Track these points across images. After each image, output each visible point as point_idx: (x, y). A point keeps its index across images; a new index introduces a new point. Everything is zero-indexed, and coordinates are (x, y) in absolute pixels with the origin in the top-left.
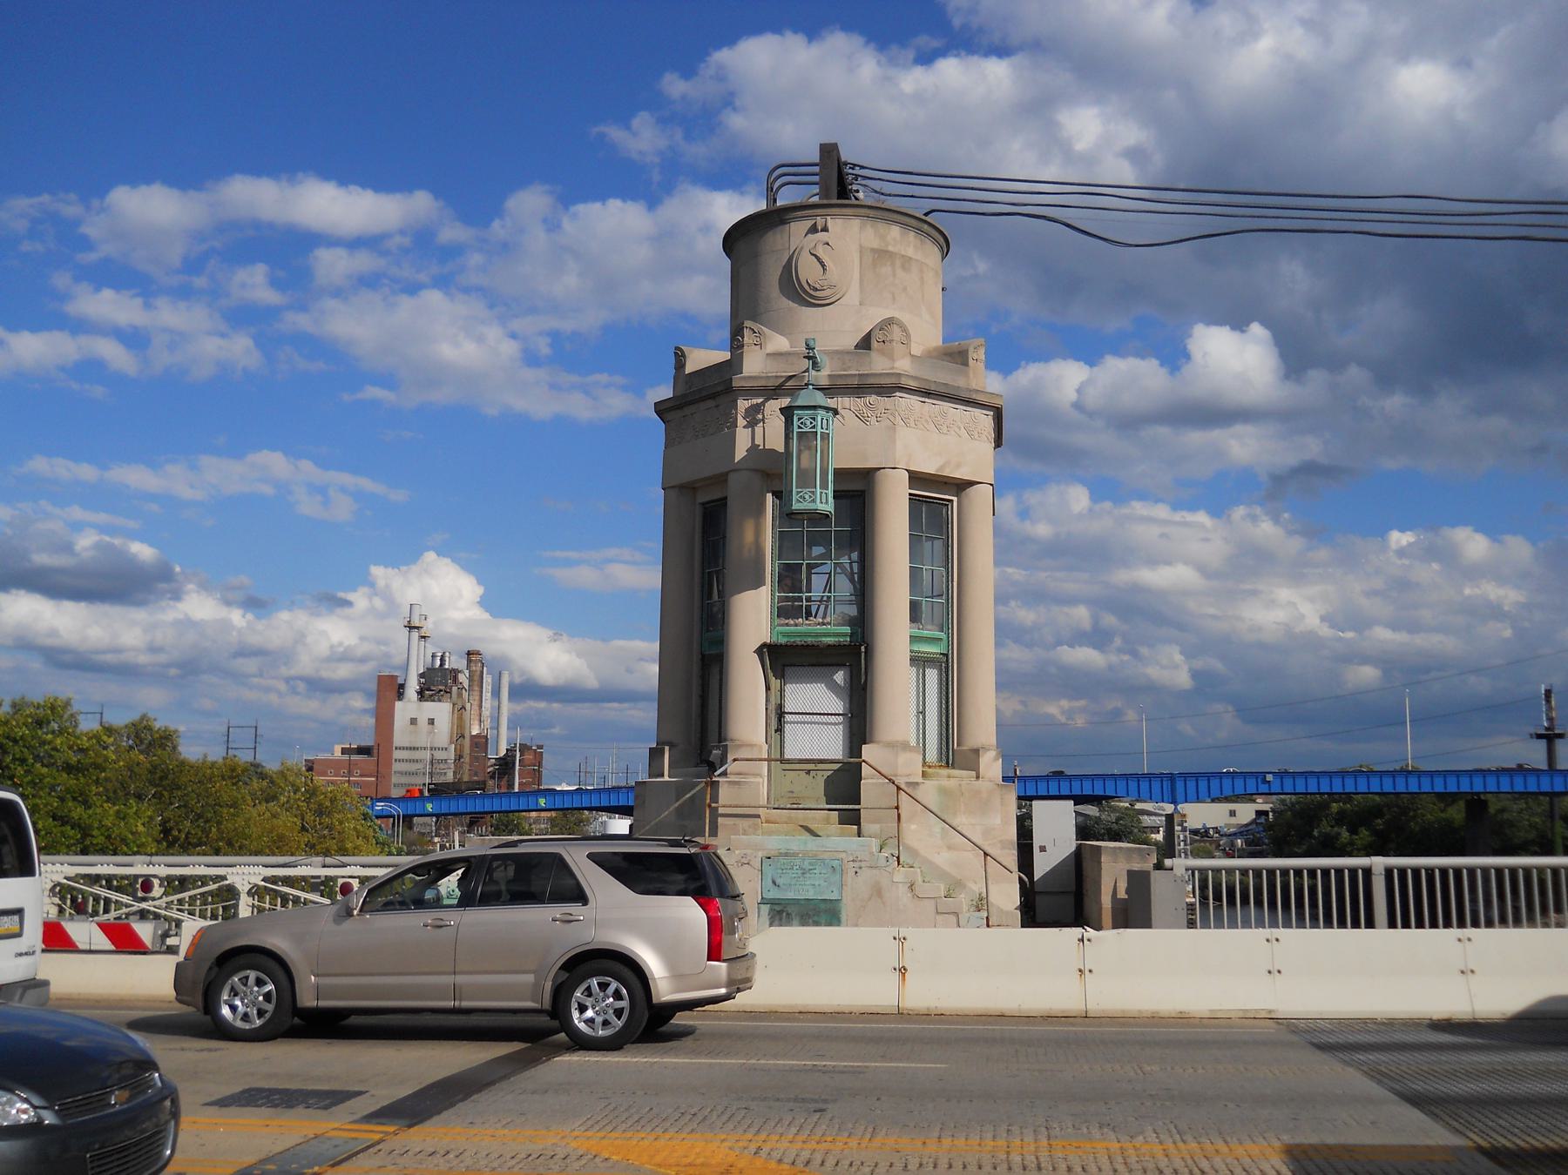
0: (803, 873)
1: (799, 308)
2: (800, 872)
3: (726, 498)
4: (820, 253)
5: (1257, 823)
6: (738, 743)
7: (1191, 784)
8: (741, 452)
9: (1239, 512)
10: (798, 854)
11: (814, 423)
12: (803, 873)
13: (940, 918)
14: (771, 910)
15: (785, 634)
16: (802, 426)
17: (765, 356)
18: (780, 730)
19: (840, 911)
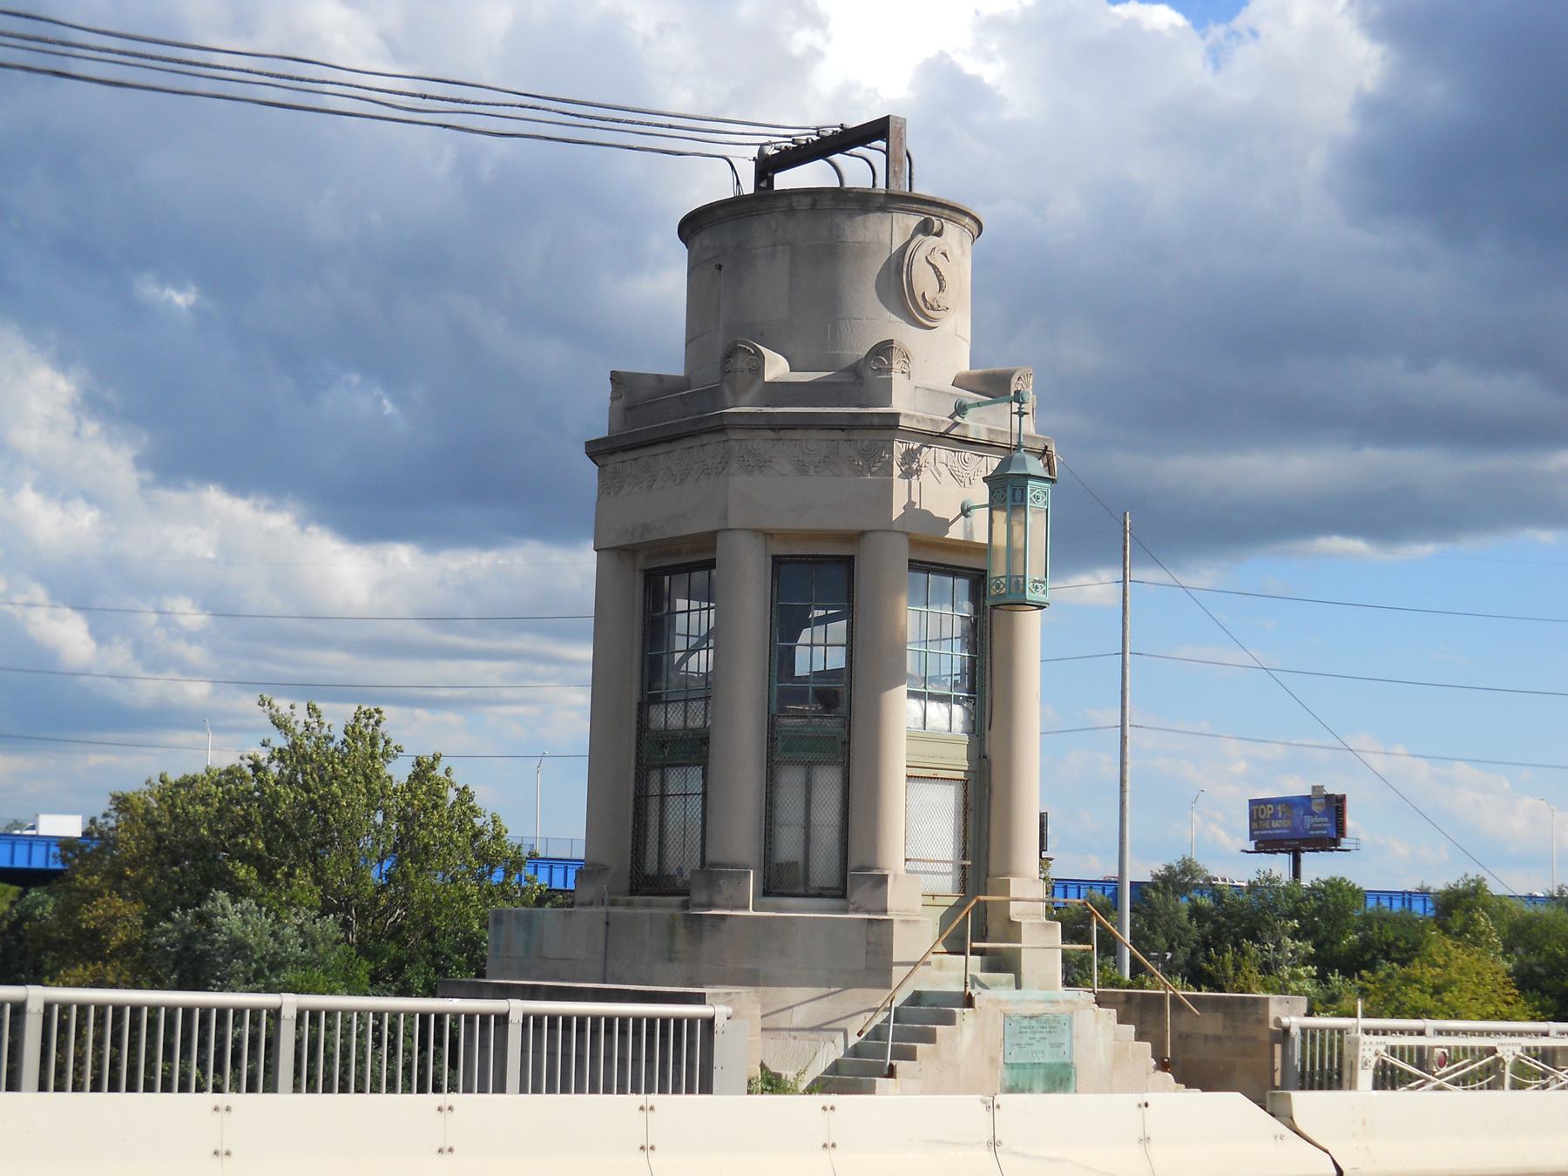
8: (897, 511)
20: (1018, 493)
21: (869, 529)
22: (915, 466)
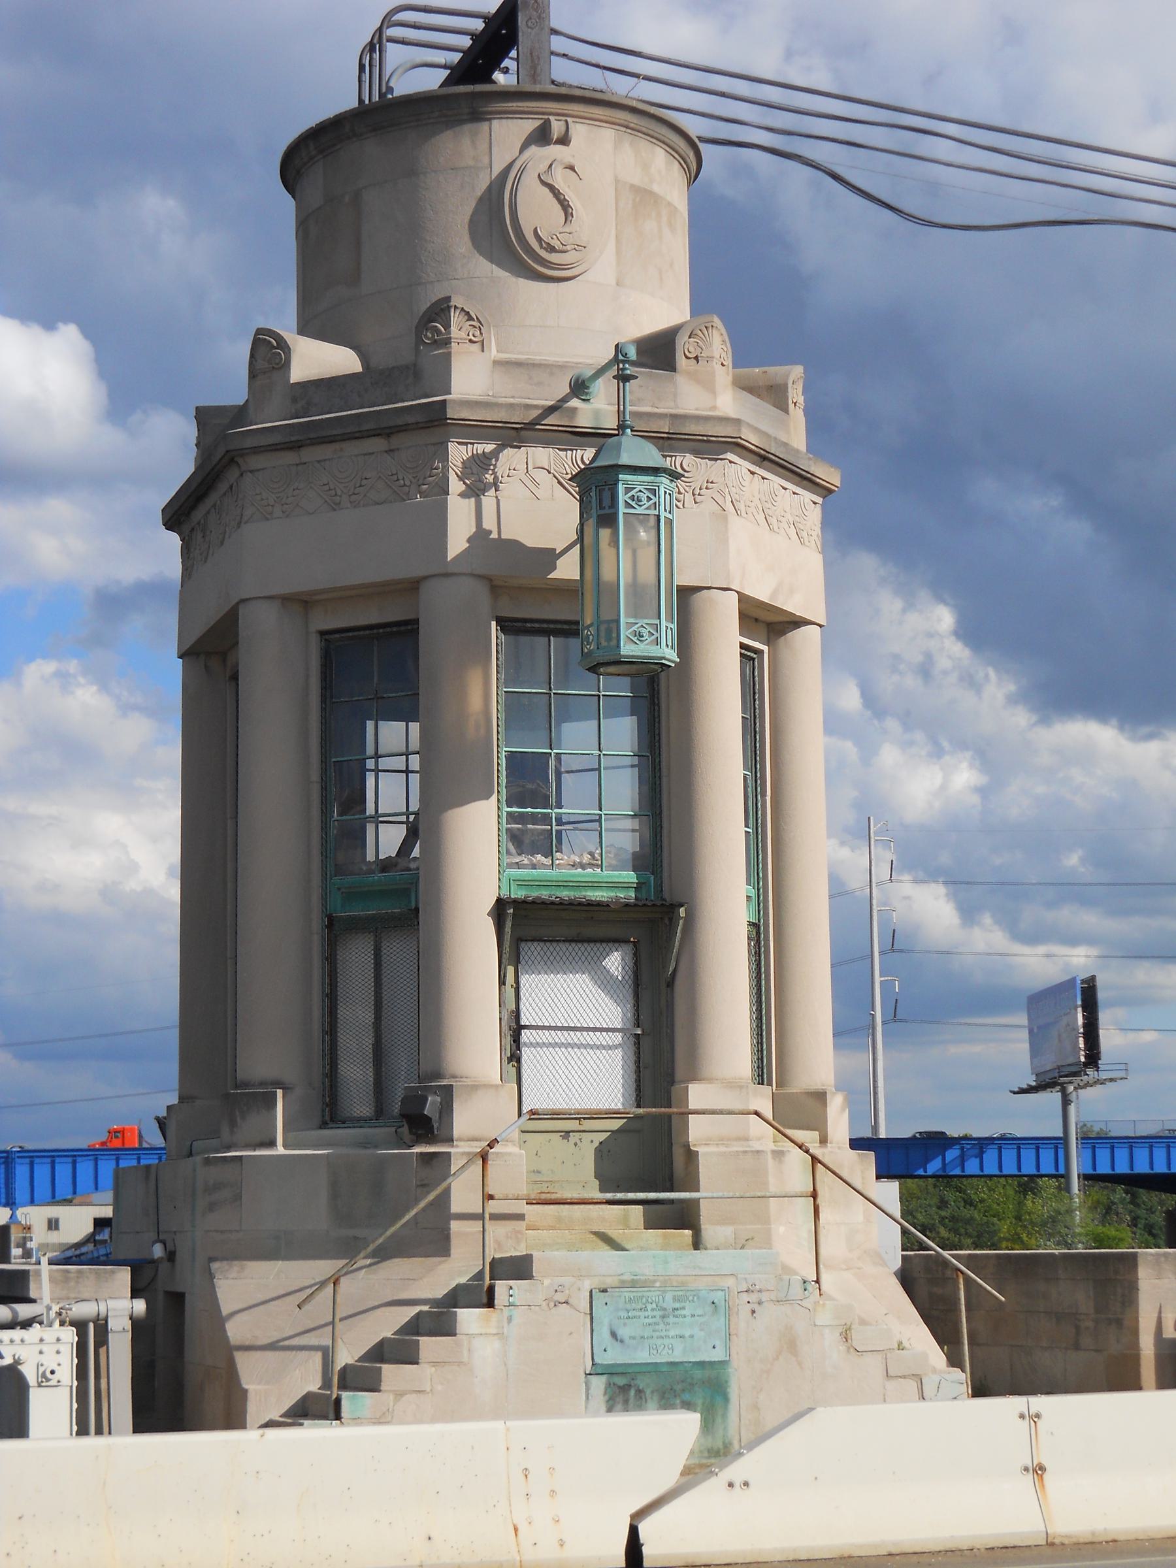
0: (663, 1317)
1: (513, 279)
2: (658, 1313)
3: (416, 621)
4: (560, 185)
5: (96, 1242)
6: (469, 1082)
7: (42, 1171)
8: (457, 542)
9: (38, 671)
10: (655, 1281)
11: (655, 499)
12: (663, 1317)
13: (891, 1385)
14: (608, 1385)
15: (523, 883)
16: (633, 504)
17: (491, 364)
18: (515, 1058)
19: (727, 1382)
20: (607, 495)
21: (426, 574)
22: (489, 478)
